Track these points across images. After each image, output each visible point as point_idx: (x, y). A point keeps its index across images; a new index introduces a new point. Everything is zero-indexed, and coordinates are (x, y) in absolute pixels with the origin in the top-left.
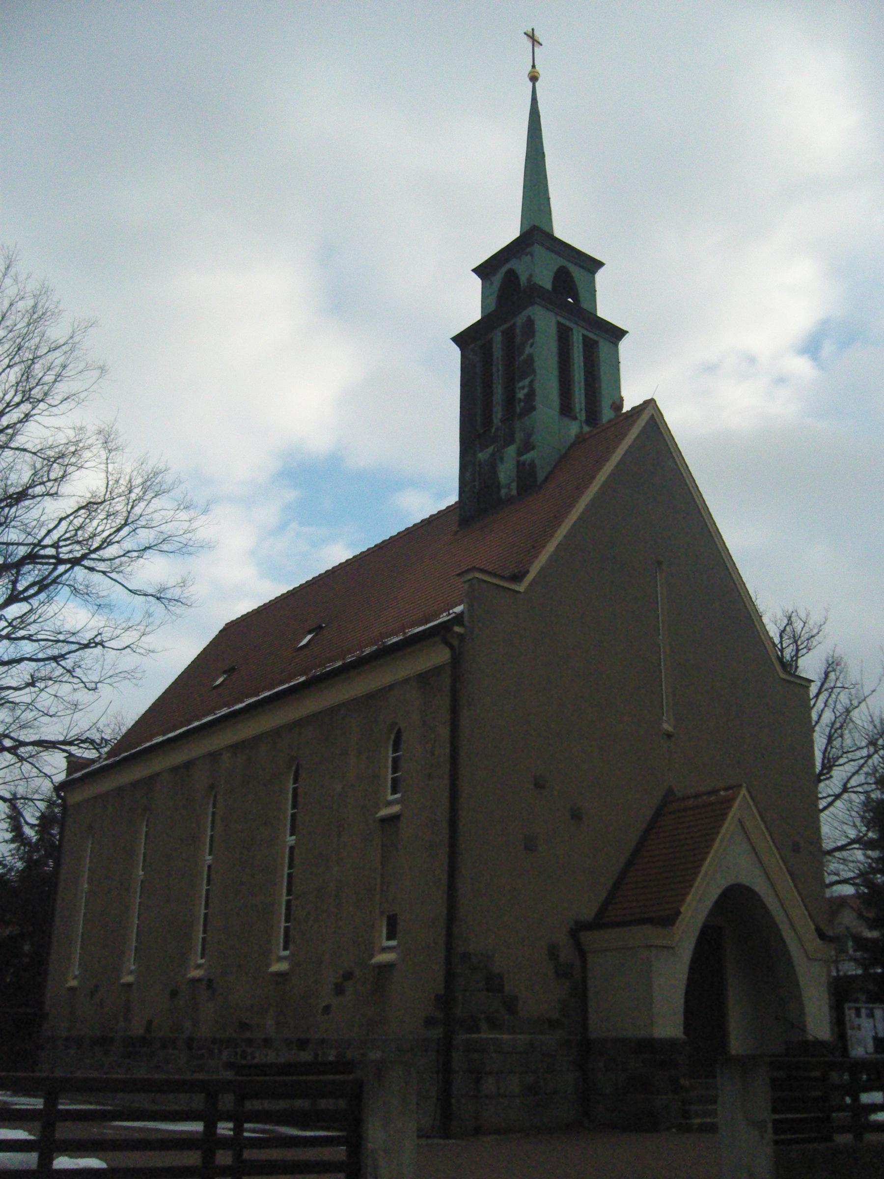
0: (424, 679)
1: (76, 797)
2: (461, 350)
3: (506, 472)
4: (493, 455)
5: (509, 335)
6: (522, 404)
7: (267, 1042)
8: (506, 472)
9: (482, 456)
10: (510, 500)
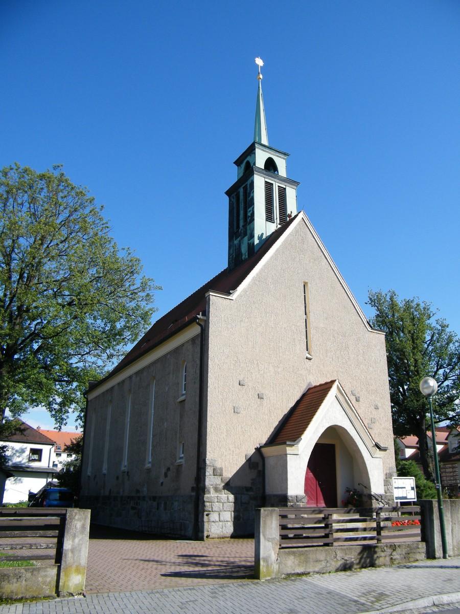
1: (92, 396)
3: (244, 249)
4: (240, 241)
5: (245, 189)
8: (244, 249)
9: (236, 242)
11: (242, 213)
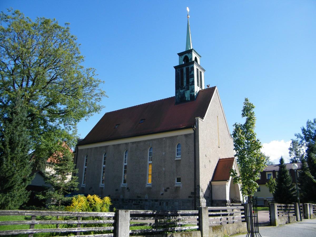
0: (186, 136)
2: (175, 69)
5: (187, 69)
6: (191, 83)
7: (146, 200)
10: (188, 101)
11: (185, 80)
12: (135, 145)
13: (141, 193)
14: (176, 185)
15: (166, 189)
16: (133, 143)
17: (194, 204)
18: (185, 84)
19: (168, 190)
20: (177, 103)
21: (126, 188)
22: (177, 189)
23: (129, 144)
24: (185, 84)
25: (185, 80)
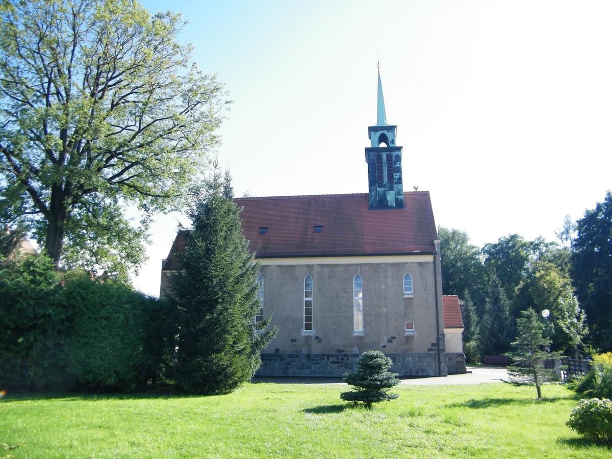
0: (420, 264)
5: (389, 157)
10: (392, 207)
12: (326, 270)
13: (344, 346)
14: (406, 334)
15: (390, 339)
16: (323, 266)
17: (437, 359)
18: (386, 179)
19: (394, 341)
20: (372, 208)
21: (314, 338)
22: (409, 339)
23: (314, 268)
24: (386, 179)
25: (385, 173)
